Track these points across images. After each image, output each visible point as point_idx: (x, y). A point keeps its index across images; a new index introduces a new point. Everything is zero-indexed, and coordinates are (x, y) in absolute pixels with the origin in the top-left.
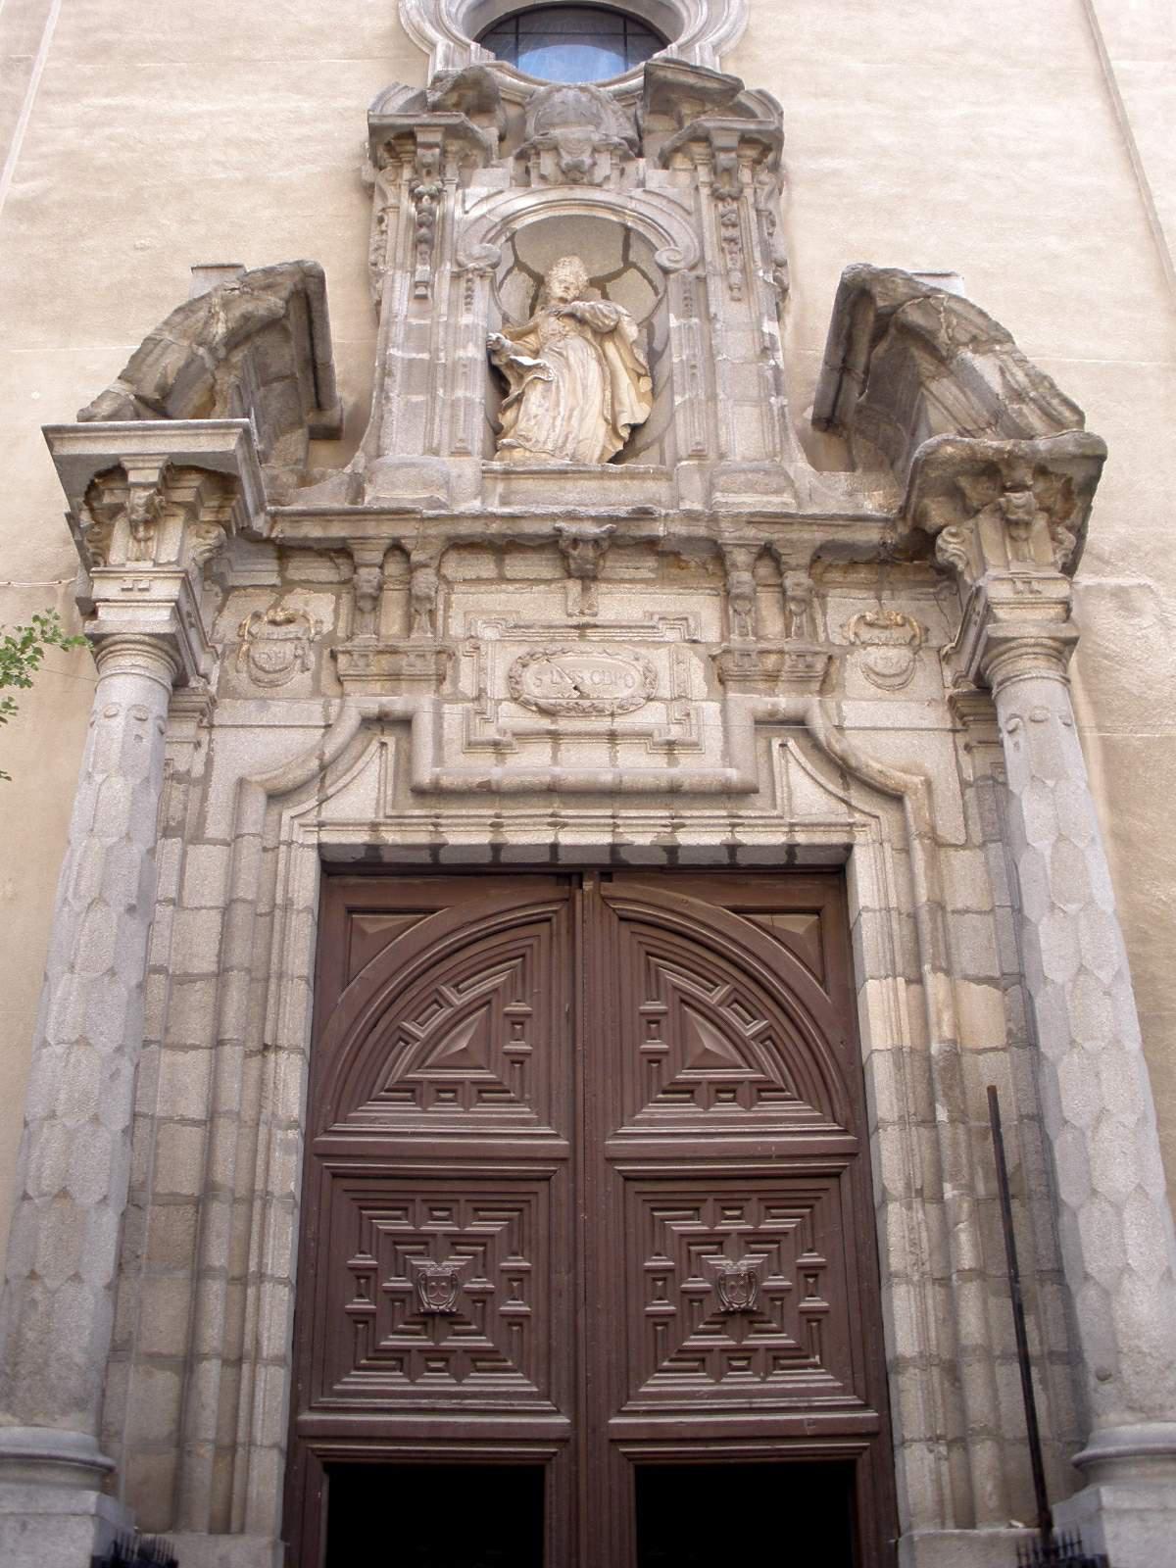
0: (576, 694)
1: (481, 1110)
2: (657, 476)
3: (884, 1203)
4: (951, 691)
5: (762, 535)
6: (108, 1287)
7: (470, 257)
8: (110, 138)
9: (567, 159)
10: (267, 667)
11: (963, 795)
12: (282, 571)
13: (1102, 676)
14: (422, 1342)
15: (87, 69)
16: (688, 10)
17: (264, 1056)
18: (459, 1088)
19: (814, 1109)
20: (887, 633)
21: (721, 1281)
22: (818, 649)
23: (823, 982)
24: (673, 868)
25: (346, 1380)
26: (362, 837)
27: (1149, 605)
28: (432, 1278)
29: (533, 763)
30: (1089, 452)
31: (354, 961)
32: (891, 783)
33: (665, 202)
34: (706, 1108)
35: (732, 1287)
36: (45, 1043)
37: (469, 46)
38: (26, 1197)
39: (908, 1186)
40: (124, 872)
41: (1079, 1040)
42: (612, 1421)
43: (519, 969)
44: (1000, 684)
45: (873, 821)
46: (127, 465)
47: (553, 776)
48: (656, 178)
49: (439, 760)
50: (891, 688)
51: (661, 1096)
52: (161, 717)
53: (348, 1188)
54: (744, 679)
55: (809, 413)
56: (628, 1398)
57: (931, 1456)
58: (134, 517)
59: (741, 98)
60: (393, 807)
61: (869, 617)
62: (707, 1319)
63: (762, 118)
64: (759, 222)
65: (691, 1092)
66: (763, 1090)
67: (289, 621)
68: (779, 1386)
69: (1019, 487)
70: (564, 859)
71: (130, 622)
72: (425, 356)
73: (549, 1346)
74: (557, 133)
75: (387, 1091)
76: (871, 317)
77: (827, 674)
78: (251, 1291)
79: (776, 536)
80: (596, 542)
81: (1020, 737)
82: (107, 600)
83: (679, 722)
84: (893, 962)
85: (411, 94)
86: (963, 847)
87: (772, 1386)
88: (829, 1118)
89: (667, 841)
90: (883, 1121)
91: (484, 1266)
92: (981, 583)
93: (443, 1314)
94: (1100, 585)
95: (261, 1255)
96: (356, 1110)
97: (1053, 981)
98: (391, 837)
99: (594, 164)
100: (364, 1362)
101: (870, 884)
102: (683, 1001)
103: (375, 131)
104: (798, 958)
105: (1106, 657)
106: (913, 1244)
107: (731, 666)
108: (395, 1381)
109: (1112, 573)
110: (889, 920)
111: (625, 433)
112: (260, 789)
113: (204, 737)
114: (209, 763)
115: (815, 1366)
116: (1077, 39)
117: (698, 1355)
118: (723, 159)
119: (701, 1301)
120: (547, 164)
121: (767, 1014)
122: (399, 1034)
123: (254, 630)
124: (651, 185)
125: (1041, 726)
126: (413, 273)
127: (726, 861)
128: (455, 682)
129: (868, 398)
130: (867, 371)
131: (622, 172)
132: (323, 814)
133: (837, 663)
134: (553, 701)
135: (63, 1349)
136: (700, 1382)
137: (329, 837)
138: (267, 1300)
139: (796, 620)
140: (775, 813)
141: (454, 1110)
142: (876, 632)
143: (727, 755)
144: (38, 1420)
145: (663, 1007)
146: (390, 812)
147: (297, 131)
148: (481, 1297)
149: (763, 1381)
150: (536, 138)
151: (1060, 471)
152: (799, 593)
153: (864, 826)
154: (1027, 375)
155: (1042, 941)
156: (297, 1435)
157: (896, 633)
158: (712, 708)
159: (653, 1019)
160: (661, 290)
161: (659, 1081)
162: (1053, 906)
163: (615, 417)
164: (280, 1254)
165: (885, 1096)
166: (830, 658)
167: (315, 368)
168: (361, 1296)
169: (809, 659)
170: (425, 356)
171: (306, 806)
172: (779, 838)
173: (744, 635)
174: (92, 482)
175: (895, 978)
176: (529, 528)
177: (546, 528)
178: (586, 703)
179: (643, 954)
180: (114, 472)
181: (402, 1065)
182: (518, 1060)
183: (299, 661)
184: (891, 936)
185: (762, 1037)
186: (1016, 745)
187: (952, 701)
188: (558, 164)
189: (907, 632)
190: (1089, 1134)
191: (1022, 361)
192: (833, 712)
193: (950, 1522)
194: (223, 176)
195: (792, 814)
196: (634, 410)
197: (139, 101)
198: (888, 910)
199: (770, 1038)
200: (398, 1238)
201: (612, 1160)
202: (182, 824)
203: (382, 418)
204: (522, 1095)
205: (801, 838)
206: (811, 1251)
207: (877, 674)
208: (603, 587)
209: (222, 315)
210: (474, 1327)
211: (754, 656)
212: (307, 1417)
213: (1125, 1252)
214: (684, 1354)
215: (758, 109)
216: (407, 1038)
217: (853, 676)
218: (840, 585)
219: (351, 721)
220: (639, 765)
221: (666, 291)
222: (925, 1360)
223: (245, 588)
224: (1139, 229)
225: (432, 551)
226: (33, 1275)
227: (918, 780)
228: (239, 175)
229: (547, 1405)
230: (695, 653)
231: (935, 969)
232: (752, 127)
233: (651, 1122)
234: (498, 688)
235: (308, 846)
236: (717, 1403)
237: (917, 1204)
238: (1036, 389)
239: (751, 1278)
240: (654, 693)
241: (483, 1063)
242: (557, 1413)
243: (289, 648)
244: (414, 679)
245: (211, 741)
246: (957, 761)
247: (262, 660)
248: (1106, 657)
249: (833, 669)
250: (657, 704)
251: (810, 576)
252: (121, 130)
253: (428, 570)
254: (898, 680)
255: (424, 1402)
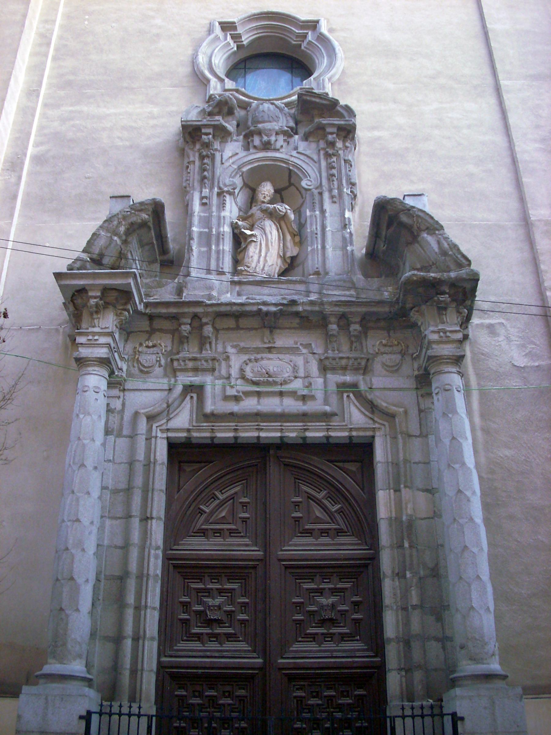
0: (267, 376)
1: (230, 540)
2: (301, 282)
3: (384, 578)
4: (416, 373)
5: (341, 310)
6: (89, 613)
7: (226, 186)
8: (73, 126)
9: (265, 138)
10: (146, 365)
11: (419, 415)
12: (151, 325)
13: (480, 363)
14: (207, 631)
15: (62, 93)
16: (318, 59)
17: (147, 521)
18: (222, 532)
19: (359, 540)
20: (391, 348)
21: (322, 607)
22: (363, 356)
23: (363, 490)
24: (305, 446)
25: (178, 645)
26: (184, 434)
27: (502, 331)
28: (212, 606)
29: (250, 405)
30: (472, 278)
31: (181, 483)
32: (390, 411)
33: (306, 157)
34: (317, 539)
35: (326, 610)
36: (63, 521)
37: (224, 80)
38: (57, 580)
39: (393, 572)
40: (92, 453)
41: (457, 518)
42: (279, 661)
43: (245, 484)
44: (433, 374)
45: (383, 427)
46: (87, 288)
47: (258, 410)
48: (302, 146)
49: (214, 403)
50: (392, 372)
51: (299, 535)
52: (105, 391)
53: (182, 570)
54: (334, 369)
55: (364, 251)
56: (286, 652)
57: (399, 676)
58: (91, 310)
59: (339, 108)
60: (196, 422)
61: (384, 342)
62: (316, 622)
63: (347, 119)
64: (345, 165)
65: (311, 533)
66: (339, 532)
67: (154, 346)
68: (343, 648)
69: (443, 293)
70: (262, 442)
71: (91, 353)
72: (206, 230)
73: (256, 632)
74: (260, 126)
75: (194, 533)
76: (387, 218)
77: (366, 366)
78: (143, 612)
79: (346, 310)
80: (275, 313)
81: (440, 396)
82: (82, 344)
83: (307, 387)
84: (389, 483)
85: (199, 109)
86: (418, 436)
87: (341, 648)
88: (364, 544)
89: (302, 435)
90: (384, 546)
91: (231, 601)
92: (426, 333)
93: (215, 620)
94: (482, 323)
95: (146, 598)
96: (182, 540)
97: (448, 496)
98: (195, 434)
99: (276, 140)
100: (185, 638)
101: (380, 453)
102: (308, 497)
103: (183, 127)
104: (355, 481)
105: (483, 354)
106: (395, 595)
107: (328, 364)
108: (197, 645)
109: (488, 318)
110: (388, 467)
111: (289, 261)
112: (143, 416)
113: (121, 394)
114: (123, 405)
115: (357, 640)
116: (486, 70)
117: (312, 636)
118: (330, 137)
119: (314, 615)
120: (257, 141)
121: (341, 502)
122: (198, 511)
123: (140, 350)
124: (300, 150)
125: (449, 392)
126: (201, 192)
127: (325, 442)
128: (220, 371)
129: (387, 248)
130: (386, 238)
131: (288, 143)
132: (169, 425)
133: (371, 361)
134: (258, 379)
135: (73, 636)
136: (313, 646)
137: (170, 434)
138: (148, 615)
139: (355, 345)
140: (344, 424)
141: (219, 540)
142: (387, 348)
143: (326, 402)
144: (65, 662)
145: (300, 500)
146: (194, 424)
147: (152, 122)
148: (230, 614)
149: (337, 646)
150: (252, 128)
151: (460, 285)
152: (356, 333)
153: (379, 428)
154: (448, 244)
155: (445, 479)
156: (161, 666)
157: (395, 348)
158: (321, 381)
159: (297, 504)
160: (304, 197)
161: (299, 529)
162: (449, 465)
163: (284, 254)
164: (154, 596)
165: (385, 536)
166: (368, 360)
167: (161, 238)
168: (184, 613)
169: (359, 360)
170: (206, 230)
171: (162, 422)
172: (346, 434)
173: (333, 351)
174: (74, 293)
175: (390, 490)
176: (248, 308)
177: (255, 308)
178: (270, 379)
179: (293, 479)
180: (82, 291)
181: (200, 523)
182: (244, 520)
183: (158, 363)
184: (388, 472)
185: (339, 511)
186: (438, 399)
187: (417, 377)
188: (261, 141)
189: (399, 349)
190: (460, 555)
191: (446, 239)
192: (369, 382)
193: (405, 700)
194: (121, 144)
195: (351, 423)
196: (292, 251)
197: (85, 109)
198: (388, 463)
199: (342, 512)
200: (198, 591)
201: (280, 560)
202: (113, 429)
203: (190, 258)
204: (246, 534)
205: (354, 434)
206: (356, 595)
207: (387, 366)
208: (278, 331)
209: (123, 223)
210: (227, 625)
211: (337, 360)
212: (164, 659)
213: (471, 601)
214: (307, 635)
215: (345, 114)
216: (202, 512)
217: (377, 366)
218: (373, 328)
219: (179, 389)
220: (290, 405)
221: (306, 198)
222: (398, 640)
223: (136, 332)
224: (508, 160)
225: (209, 318)
226: (61, 609)
227: (401, 410)
228: (127, 143)
229: (255, 655)
230: (315, 358)
231: (405, 487)
232: (343, 123)
233: (296, 545)
234: (234, 372)
235: (163, 438)
236: (319, 655)
237: (396, 579)
238: (452, 251)
239: (333, 606)
240: (297, 375)
241: (231, 522)
242: (258, 658)
243: (154, 357)
244: (204, 370)
245: (124, 395)
246: (418, 402)
247: (144, 362)
248: (483, 354)
249: (369, 364)
250: (298, 379)
251: (361, 326)
252: (78, 122)
253: (208, 326)
254: (395, 368)
255: (208, 654)
